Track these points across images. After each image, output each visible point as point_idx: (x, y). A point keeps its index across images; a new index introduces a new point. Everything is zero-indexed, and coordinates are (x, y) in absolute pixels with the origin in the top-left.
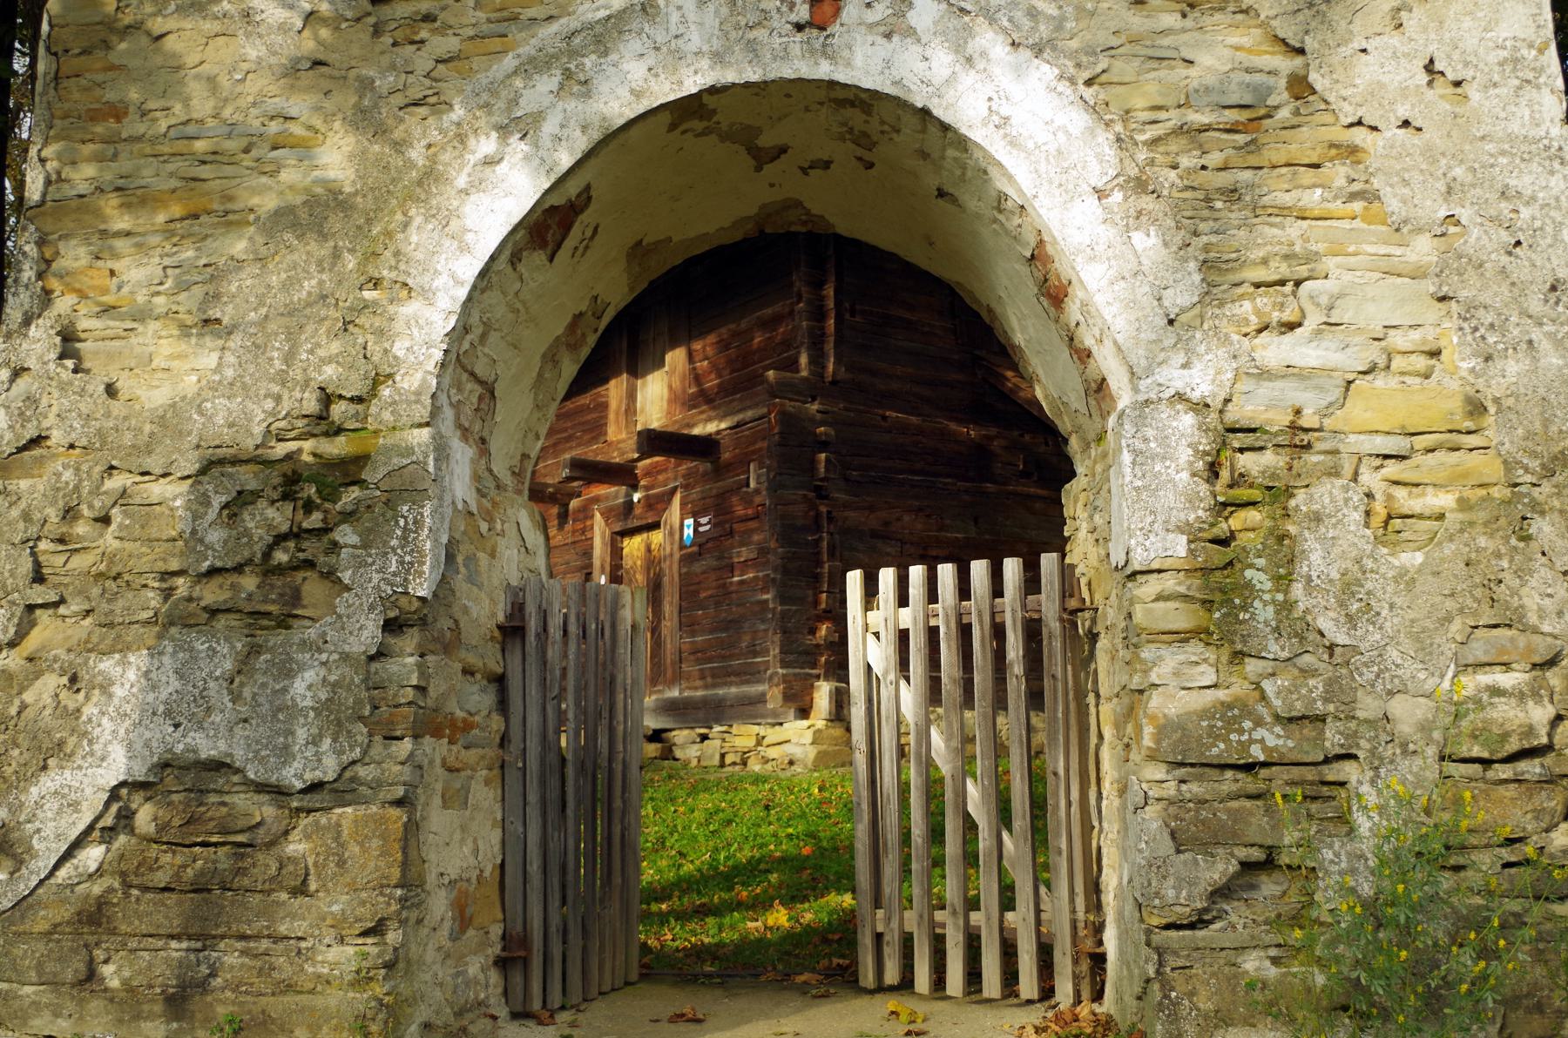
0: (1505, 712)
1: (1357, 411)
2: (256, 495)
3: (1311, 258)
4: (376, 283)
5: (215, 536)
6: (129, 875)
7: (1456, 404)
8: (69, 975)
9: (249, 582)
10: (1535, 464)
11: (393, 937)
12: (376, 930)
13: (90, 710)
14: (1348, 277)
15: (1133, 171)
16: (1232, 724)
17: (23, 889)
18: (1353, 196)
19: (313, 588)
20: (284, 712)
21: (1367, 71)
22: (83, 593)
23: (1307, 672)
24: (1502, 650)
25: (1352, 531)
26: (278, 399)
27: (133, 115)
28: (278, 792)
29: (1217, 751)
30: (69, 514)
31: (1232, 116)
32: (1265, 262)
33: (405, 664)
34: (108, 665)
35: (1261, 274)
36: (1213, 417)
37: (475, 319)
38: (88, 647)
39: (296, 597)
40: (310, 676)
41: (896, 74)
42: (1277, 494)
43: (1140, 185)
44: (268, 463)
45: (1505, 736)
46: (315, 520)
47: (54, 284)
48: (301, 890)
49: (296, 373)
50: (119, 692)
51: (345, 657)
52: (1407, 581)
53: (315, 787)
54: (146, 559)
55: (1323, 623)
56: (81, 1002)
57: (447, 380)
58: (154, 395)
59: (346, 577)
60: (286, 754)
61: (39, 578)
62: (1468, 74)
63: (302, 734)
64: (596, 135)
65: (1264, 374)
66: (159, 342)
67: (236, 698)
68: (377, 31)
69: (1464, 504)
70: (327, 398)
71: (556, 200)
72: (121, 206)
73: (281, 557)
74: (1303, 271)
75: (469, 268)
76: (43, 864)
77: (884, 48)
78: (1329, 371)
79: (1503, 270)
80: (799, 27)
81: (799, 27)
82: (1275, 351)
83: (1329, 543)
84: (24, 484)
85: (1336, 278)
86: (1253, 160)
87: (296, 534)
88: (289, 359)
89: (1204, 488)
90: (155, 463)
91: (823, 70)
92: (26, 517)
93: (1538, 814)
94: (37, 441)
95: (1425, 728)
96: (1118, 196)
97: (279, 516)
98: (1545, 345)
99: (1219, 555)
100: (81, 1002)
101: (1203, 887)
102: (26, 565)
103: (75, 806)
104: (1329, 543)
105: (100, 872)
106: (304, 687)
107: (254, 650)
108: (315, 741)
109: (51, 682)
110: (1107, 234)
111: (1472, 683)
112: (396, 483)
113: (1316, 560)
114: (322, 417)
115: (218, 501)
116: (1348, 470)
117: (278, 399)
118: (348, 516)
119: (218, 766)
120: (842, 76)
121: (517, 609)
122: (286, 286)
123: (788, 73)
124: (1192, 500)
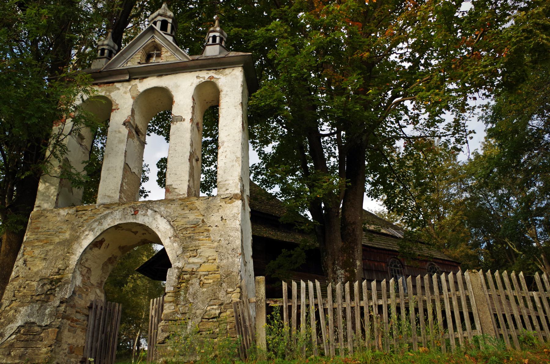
0: (213, 312)
1: (202, 269)
4: (69, 253)
5: (39, 290)
6: (17, 339)
7: (216, 267)
9: (43, 296)
11: (53, 347)
12: (50, 346)
13: (17, 315)
16: (174, 314)
17: (2, 341)
19: (52, 297)
20: (44, 315)
21: (213, 218)
22: (20, 298)
23: (186, 307)
28: (40, 326)
29: (171, 318)
30: (20, 287)
31: (192, 226)
33: (62, 308)
34: (21, 309)
35: (191, 249)
36: (180, 270)
39: (49, 298)
40: (49, 310)
42: (188, 281)
43: (176, 236)
47: (25, 253)
48: (42, 341)
49: (55, 266)
50: (22, 312)
51: (54, 307)
52: (203, 293)
53: (46, 326)
54: (29, 293)
55: (190, 299)
56: (7, 358)
57: (77, 267)
58: (35, 269)
60: (43, 321)
61: (14, 296)
63: (46, 318)
65: (189, 263)
66: (38, 262)
67: (38, 313)
68: (76, 216)
69: (214, 282)
70: (59, 269)
71: (97, 240)
72: (279, 218)
73: (48, 293)
75: (82, 250)
76: (6, 338)
77: (143, 218)
78: (198, 263)
82: (192, 260)
83: (193, 288)
85: (202, 249)
87: (51, 289)
88: (55, 264)
89: (177, 280)
90: (33, 279)
91: (135, 221)
92: (14, 287)
93: (214, 326)
94: (18, 276)
95: (200, 314)
97: (49, 287)
98: (230, 258)
99: (178, 290)
100: (7, 358)
101: (164, 337)
102: (13, 294)
104: (193, 288)
106: (47, 311)
107: (42, 306)
108: (47, 319)
109: (13, 311)
110: (170, 243)
111: (209, 308)
113: (191, 290)
114: (58, 272)
115: (41, 284)
116: (198, 277)
118: (58, 286)
120: (137, 222)
121: (92, 304)
122: (56, 253)
124: (175, 282)
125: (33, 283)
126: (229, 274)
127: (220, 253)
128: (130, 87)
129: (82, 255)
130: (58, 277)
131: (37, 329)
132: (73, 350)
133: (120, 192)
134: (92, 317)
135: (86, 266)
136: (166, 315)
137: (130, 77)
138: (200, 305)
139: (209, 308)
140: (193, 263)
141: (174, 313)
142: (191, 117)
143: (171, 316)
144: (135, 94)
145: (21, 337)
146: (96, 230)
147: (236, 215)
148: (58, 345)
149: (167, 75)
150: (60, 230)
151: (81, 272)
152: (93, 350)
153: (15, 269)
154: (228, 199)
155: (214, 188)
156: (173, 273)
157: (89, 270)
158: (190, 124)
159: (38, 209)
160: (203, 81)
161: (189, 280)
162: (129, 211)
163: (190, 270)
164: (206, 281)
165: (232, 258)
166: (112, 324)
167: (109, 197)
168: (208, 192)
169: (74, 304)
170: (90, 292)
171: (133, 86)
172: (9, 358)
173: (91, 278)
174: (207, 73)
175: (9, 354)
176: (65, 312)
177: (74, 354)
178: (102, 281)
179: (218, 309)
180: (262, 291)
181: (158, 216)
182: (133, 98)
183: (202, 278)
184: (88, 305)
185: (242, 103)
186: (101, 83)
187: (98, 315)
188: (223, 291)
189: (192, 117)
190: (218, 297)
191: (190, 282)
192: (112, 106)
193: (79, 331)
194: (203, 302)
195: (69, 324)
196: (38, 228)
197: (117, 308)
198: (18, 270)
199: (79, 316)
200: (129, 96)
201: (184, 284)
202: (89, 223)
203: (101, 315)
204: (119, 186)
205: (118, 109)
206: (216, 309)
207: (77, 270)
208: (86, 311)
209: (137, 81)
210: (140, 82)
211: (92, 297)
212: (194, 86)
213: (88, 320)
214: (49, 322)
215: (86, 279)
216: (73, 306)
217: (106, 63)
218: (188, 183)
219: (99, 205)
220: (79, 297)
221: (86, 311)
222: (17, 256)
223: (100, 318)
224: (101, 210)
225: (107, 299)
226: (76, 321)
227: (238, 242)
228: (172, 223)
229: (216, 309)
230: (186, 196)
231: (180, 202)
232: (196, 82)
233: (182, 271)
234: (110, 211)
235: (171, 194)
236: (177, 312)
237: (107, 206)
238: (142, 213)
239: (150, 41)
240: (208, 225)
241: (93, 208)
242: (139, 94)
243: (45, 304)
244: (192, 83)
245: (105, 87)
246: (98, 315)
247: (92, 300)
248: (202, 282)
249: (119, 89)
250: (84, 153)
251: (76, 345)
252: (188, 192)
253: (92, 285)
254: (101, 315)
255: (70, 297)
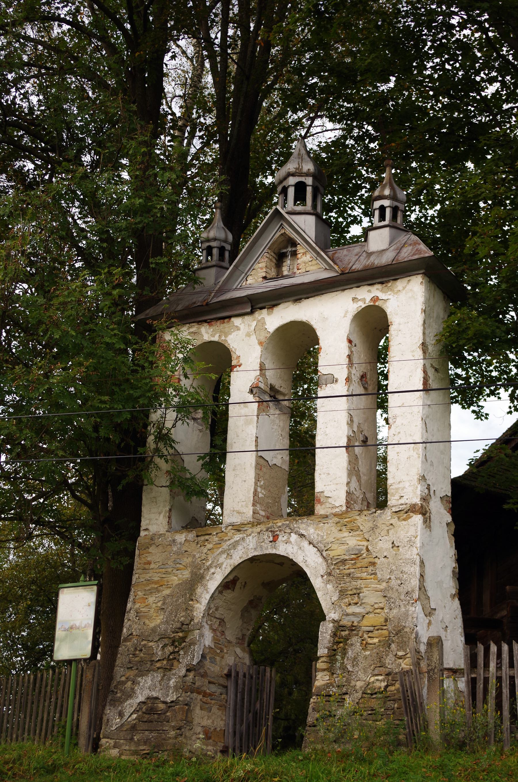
0: (377, 684)
1: (365, 622)
2: (168, 644)
3: (360, 588)
4: (192, 600)
5: (160, 653)
8: (129, 738)
9: (165, 662)
10: (394, 632)
13: (136, 688)
14: (367, 592)
15: (329, 571)
18: (372, 574)
19: (175, 663)
20: (168, 687)
21: (381, 545)
22: (136, 665)
23: (344, 677)
24: (380, 672)
25: (358, 647)
26: (173, 625)
27: (153, 563)
30: (136, 649)
32: (351, 590)
34: (139, 679)
37: (212, 606)
38: (137, 676)
39: (172, 665)
40: (173, 680)
41: (287, 551)
42: (346, 639)
43: (330, 574)
44: (170, 638)
45: (375, 689)
46: (177, 649)
48: (168, 722)
51: (179, 676)
52: (366, 658)
53: (172, 702)
55: (348, 667)
56: (130, 743)
57: (205, 620)
59: (181, 661)
60: (168, 695)
62: (400, 544)
63: (171, 692)
64: (232, 567)
65: (347, 615)
68: (197, 543)
69: (380, 641)
71: (227, 580)
73: (171, 657)
74: (358, 591)
75: (208, 596)
79: (397, 590)
80: (271, 542)
81: (271, 542)
84: (128, 643)
86: (354, 567)
87: (174, 652)
88: (175, 616)
90: (150, 639)
91: (274, 551)
92: (128, 650)
94: (131, 634)
95: (361, 687)
96: (326, 577)
97: (171, 649)
100: (130, 743)
103: (132, 706)
105: (135, 719)
106: (172, 683)
107: (164, 675)
108: (173, 693)
109: (129, 683)
110: (322, 585)
111: (372, 679)
112: (191, 641)
113: (350, 654)
115: (161, 646)
117: (173, 625)
118: (182, 648)
119: (157, 698)
121: (230, 671)
122: (176, 601)
123: (268, 552)
124: (329, 642)
125: (151, 644)
126: (400, 631)
127: (390, 598)
128: (254, 323)
129: (208, 603)
130: (181, 634)
131: (162, 706)
132: (209, 735)
133: (254, 505)
134: (232, 690)
135: (217, 616)
136: (318, 688)
137: (252, 307)
138: (361, 675)
139: (372, 679)
140: (354, 614)
141: (328, 685)
142: (346, 376)
143: (324, 689)
144: (263, 336)
145: (144, 717)
146: (224, 566)
147: (413, 539)
148: (188, 728)
149: (308, 298)
150: (178, 565)
151: (211, 627)
152: (238, 735)
153: (127, 624)
154: (403, 512)
155: (488, 395)
156: (326, 629)
157: (222, 621)
158: (346, 387)
159: (146, 533)
160: (364, 306)
161: (348, 640)
162: (265, 537)
163: (350, 624)
164: (370, 641)
165: (405, 606)
166: (262, 699)
167: (239, 513)
168: (476, 409)
169: (206, 672)
170: (227, 653)
171: (259, 321)
172: (133, 743)
173: (227, 633)
174: (369, 291)
175: (132, 739)
176: (194, 684)
177: (211, 741)
178: (244, 635)
179: (384, 681)
180: (435, 657)
181: (305, 544)
182: (261, 343)
183: (366, 636)
184: (226, 672)
185: (423, 344)
186: (212, 320)
187: (240, 686)
188: (391, 655)
189: (350, 373)
190: (385, 664)
191: (349, 642)
192: (231, 361)
193: (215, 709)
194: (365, 671)
195: (201, 700)
196: (149, 563)
197: (268, 674)
198: (130, 626)
199: (213, 688)
200: (254, 340)
201: (341, 645)
202: (216, 554)
203: (244, 684)
204: (252, 495)
205: (240, 366)
206: (381, 681)
207: (205, 624)
208: (223, 681)
209: (265, 311)
210: (268, 314)
211: (230, 660)
212: (350, 316)
213: (227, 694)
214: (175, 697)
215: (219, 634)
216: (204, 675)
217: (217, 278)
218: (346, 488)
219: (227, 527)
220: (212, 662)
221: (223, 681)
222: (126, 605)
223: (243, 689)
224: (229, 534)
225: (255, 662)
226: (210, 695)
227: (415, 582)
228: (324, 553)
229: (381, 681)
230: (344, 508)
231: (336, 519)
232: (354, 308)
233: (339, 627)
234: (241, 536)
235: (323, 506)
236: (331, 684)
237: (238, 528)
238: (284, 539)
239: (278, 234)
240: (374, 555)
241: (218, 531)
242: (268, 336)
243: (168, 673)
244: (347, 312)
245: (219, 326)
246: (240, 686)
247: (231, 664)
248: (364, 642)
249: (238, 328)
250: (200, 431)
251: (212, 729)
252: (347, 502)
253: (229, 642)
254: (244, 684)
255: (198, 663)
